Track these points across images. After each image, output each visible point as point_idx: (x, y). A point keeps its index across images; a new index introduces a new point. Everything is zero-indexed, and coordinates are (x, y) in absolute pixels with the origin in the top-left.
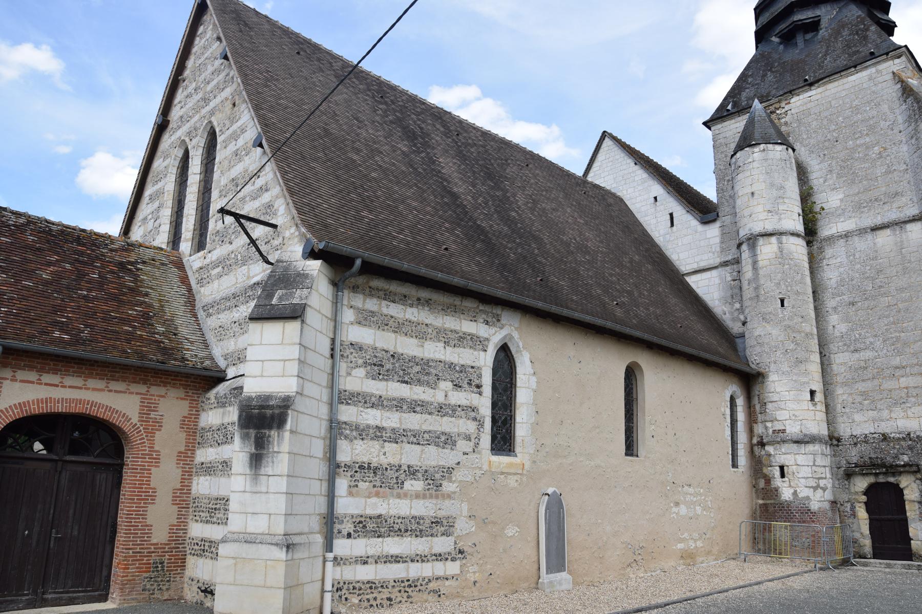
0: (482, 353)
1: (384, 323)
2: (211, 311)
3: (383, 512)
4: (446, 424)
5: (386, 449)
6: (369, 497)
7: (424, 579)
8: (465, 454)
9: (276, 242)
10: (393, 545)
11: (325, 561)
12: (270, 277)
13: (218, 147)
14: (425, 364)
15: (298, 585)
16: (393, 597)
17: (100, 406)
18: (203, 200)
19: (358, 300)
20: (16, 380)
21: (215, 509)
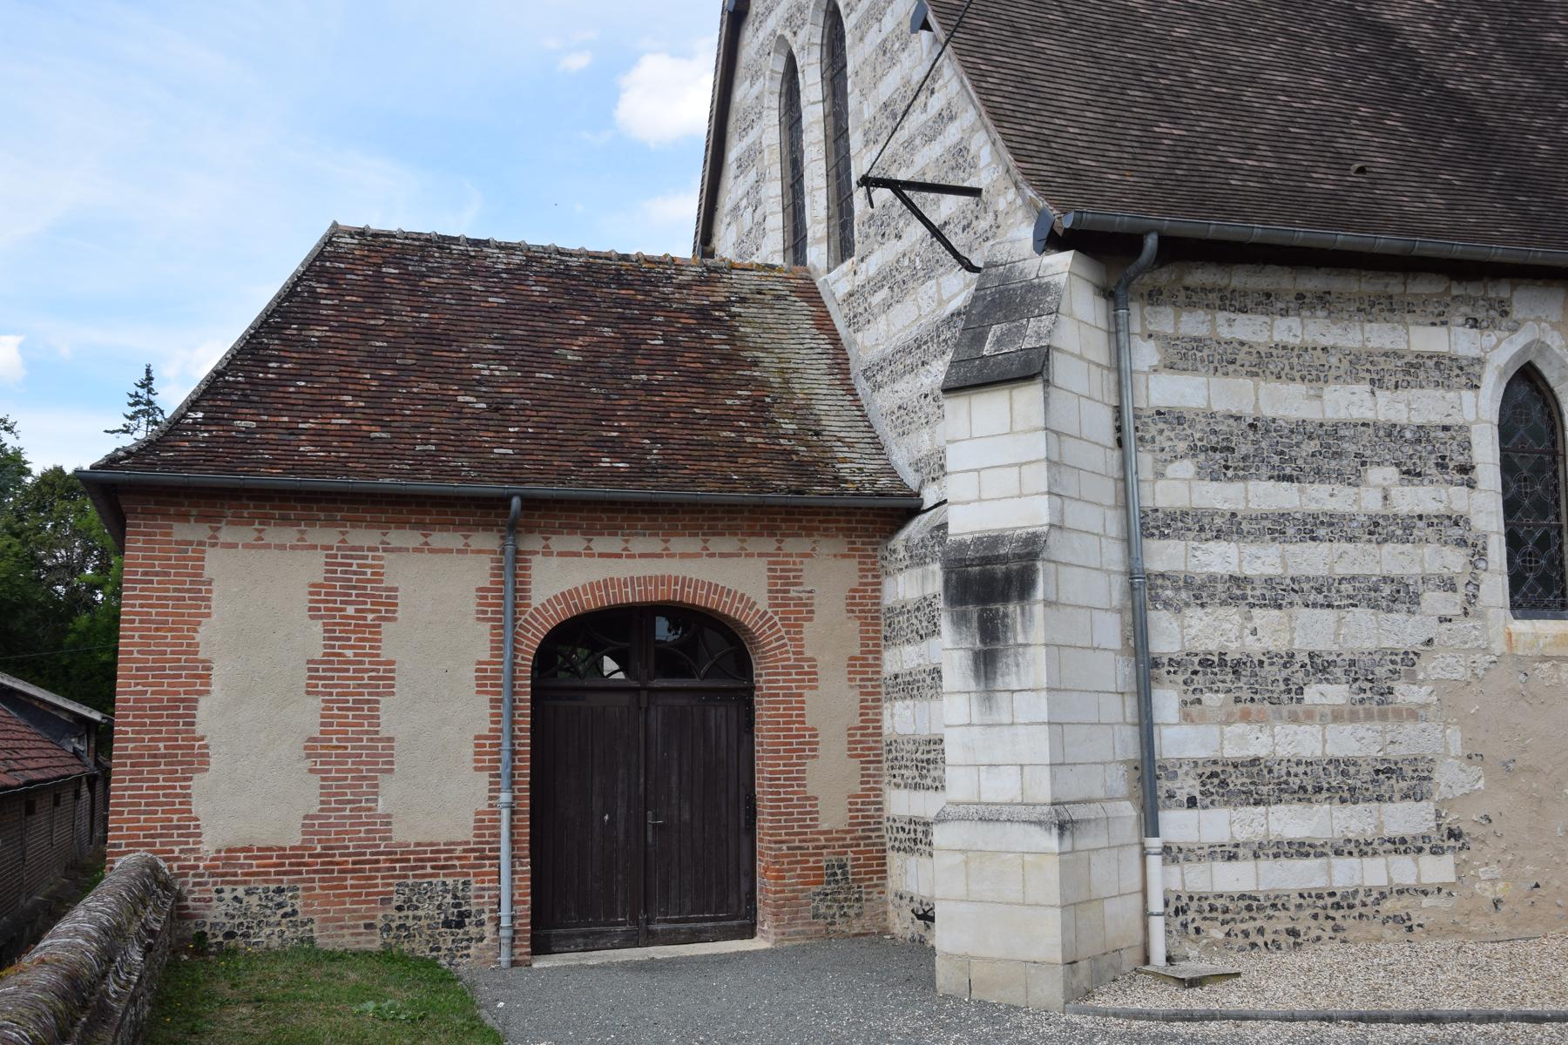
0: (1468, 395)
1: (1226, 360)
2: (879, 378)
3: (1262, 753)
4: (1392, 560)
5: (1257, 622)
6: (1228, 723)
7: (1368, 892)
8: (1442, 620)
9: (982, 225)
10: (1289, 821)
11: (1144, 854)
12: (975, 299)
13: (848, 41)
14: (1330, 436)
15: (1090, 901)
16: (1301, 927)
17: (698, 584)
18: (837, 154)
19: (1165, 320)
20: (551, 554)
21: (928, 761)
